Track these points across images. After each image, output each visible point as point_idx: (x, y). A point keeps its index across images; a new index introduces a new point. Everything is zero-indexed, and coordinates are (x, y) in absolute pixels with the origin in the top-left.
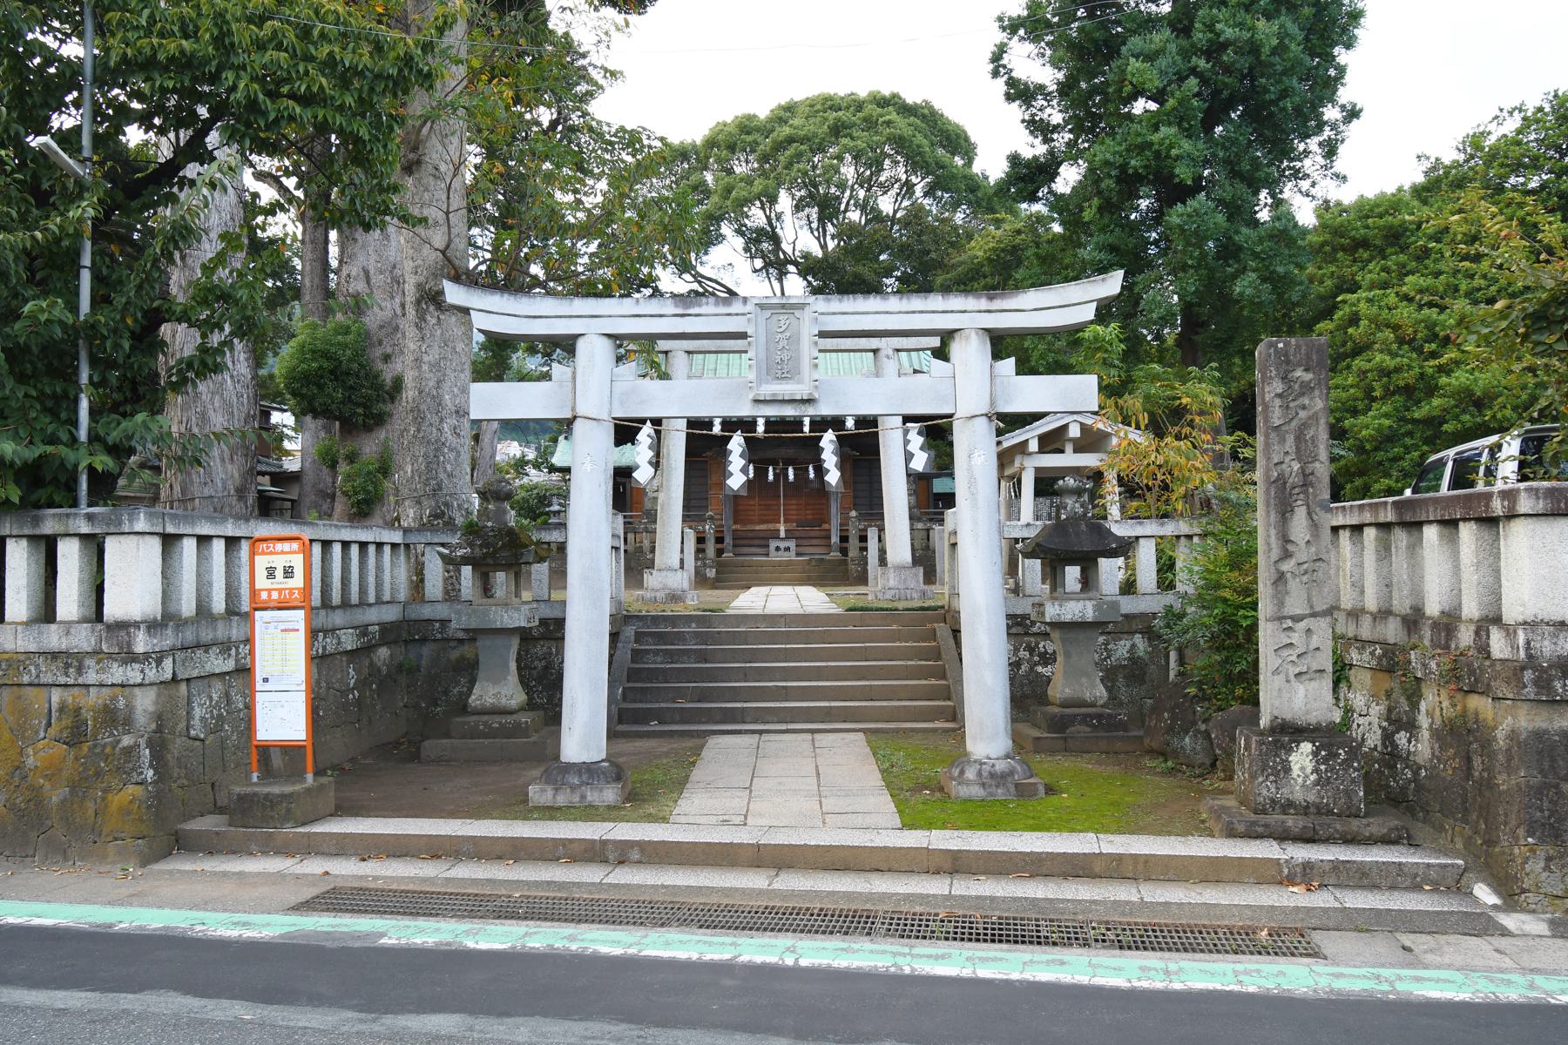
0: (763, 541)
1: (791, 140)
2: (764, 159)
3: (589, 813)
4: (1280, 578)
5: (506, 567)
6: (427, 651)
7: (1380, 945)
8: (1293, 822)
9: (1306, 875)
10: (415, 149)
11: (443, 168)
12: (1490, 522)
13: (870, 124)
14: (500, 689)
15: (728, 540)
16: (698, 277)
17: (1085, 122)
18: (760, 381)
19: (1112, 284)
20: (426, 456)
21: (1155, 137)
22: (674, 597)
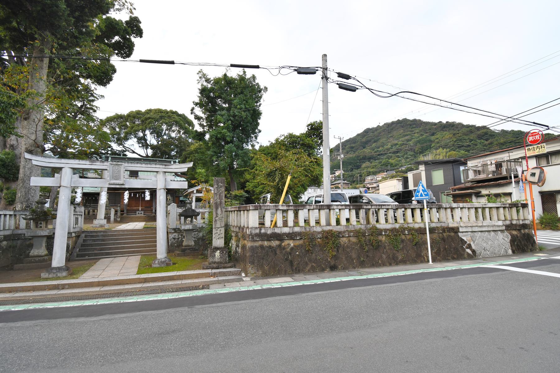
0: (135, 211)
1: (150, 118)
2: (142, 121)
3: (58, 278)
4: (216, 220)
5: (43, 220)
6: (19, 242)
7: (222, 285)
8: (215, 265)
9: (214, 275)
10: (28, 114)
11: (36, 120)
12: (247, 210)
13: (169, 117)
14: (40, 251)
15: (125, 211)
16: (124, 146)
17: (210, 126)
18: (110, 180)
19: (191, 165)
20: (25, 191)
21: (223, 131)
22: (102, 226)
